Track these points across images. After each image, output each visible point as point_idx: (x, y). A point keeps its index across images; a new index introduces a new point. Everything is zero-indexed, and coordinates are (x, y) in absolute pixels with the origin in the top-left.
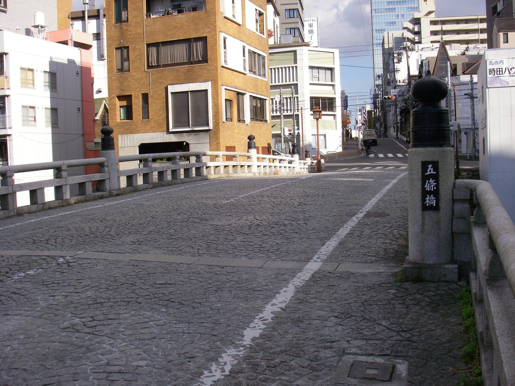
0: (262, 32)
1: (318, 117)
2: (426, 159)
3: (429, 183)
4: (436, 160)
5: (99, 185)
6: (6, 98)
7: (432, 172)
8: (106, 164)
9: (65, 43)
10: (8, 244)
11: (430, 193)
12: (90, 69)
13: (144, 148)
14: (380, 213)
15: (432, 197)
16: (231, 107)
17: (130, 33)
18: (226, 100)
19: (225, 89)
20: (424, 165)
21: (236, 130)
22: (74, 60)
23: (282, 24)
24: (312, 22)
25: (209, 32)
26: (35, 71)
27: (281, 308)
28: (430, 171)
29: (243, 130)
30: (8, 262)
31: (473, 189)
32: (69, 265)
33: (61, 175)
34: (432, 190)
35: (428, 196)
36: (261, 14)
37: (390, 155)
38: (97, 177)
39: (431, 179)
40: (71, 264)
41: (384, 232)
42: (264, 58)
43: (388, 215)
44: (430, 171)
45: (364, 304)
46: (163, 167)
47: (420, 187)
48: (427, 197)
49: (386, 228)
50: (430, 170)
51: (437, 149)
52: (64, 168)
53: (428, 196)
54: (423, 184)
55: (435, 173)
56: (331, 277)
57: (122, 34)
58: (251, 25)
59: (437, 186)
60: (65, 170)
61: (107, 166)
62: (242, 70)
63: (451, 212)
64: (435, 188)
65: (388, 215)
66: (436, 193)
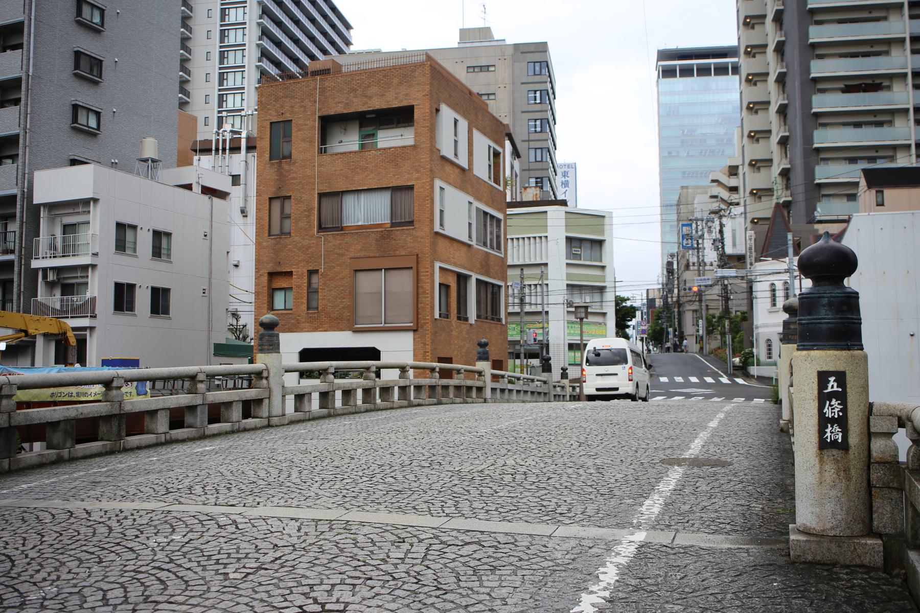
0: (497, 181)
1: (583, 315)
2: (825, 368)
3: (830, 405)
4: (842, 369)
5: (249, 408)
6: (90, 270)
7: (835, 389)
8: (265, 374)
9: (189, 187)
10: (122, 493)
11: (833, 421)
12: (153, 256)
13: (307, 355)
14: (715, 461)
15: (836, 428)
16: (448, 295)
17: (294, 175)
18: (440, 284)
19: (441, 268)
20: (823, 377)
21: (454, 333)
23: (523, 170)
24: (567, 170)
25: (418, 179)
26: (139, 228)
27: (604, 598)
28: (832, 387)
29: (464, 333)
30: (134, 520)
31: (904, 418)
32: (237, 528)
33: (197, 388)
36: (497, 155)
37: (694, 379)
38: (251, 394)
39: (834, 400)
40: (240, 526)
41: (732, 489)
42: (499, 221)
43: (731, 464)
44: (832, 387)
45: (737, 596)
46: (351, 383)
47: (815, 411)
49: (732, 483)
50: (832, 386)
51: (844, 353)
52: (201, 377)
54: (821, 407)
55: (840, 390)
56: (669, 554)
57: (282, 178)
58: (482, 170)
59: (844, 410)
60: (202, 382)
61: (267, 378)
62: (465, 239)
63: (866, 453)
65: (731, 464)
66: (842, 422)
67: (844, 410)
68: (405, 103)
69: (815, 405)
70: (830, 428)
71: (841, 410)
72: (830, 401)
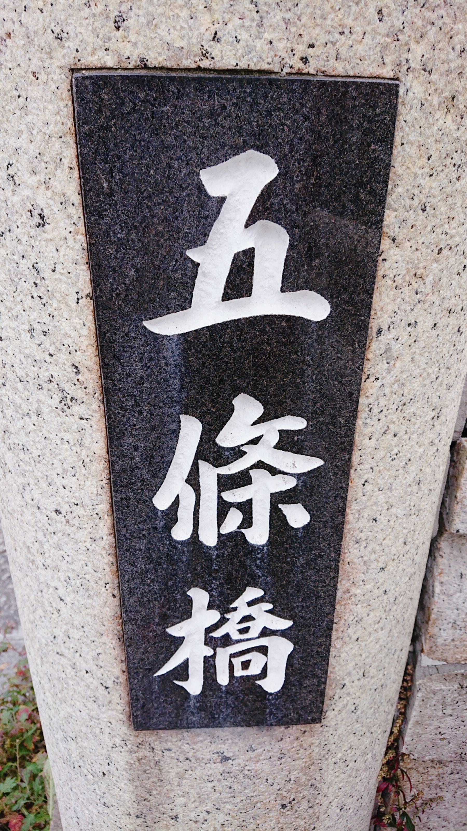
2: (164, 38)
3: (210, 451)
4: (356, 57)
7: (268, 299)
15: (254, 611)
22: (233, 410)
34: (258, 535)
35: (199, 597)
39: (247, 409)
48: (185, 612)
50: (240, 257)
53: (199, 597)
55: (313, 308)
64: (297, 516)
67: (326, 493)
68: (252, 607)
69: (74, 446)
70: (203, 615)
71: (305, 490)
72: (216, 418)
